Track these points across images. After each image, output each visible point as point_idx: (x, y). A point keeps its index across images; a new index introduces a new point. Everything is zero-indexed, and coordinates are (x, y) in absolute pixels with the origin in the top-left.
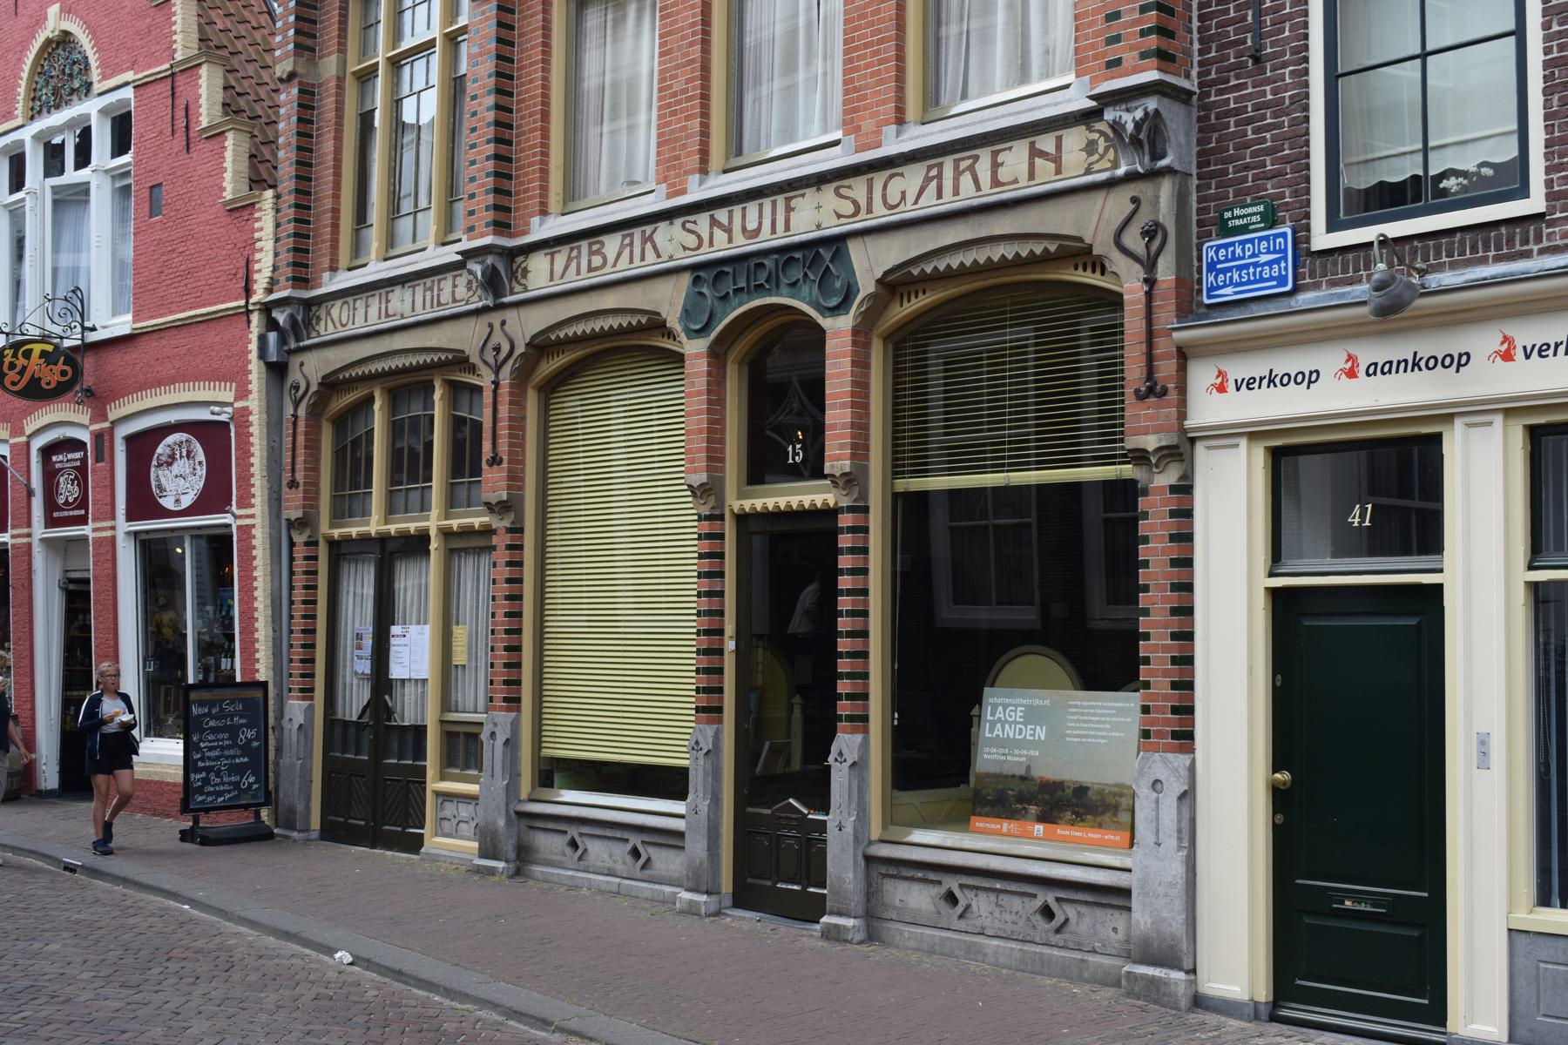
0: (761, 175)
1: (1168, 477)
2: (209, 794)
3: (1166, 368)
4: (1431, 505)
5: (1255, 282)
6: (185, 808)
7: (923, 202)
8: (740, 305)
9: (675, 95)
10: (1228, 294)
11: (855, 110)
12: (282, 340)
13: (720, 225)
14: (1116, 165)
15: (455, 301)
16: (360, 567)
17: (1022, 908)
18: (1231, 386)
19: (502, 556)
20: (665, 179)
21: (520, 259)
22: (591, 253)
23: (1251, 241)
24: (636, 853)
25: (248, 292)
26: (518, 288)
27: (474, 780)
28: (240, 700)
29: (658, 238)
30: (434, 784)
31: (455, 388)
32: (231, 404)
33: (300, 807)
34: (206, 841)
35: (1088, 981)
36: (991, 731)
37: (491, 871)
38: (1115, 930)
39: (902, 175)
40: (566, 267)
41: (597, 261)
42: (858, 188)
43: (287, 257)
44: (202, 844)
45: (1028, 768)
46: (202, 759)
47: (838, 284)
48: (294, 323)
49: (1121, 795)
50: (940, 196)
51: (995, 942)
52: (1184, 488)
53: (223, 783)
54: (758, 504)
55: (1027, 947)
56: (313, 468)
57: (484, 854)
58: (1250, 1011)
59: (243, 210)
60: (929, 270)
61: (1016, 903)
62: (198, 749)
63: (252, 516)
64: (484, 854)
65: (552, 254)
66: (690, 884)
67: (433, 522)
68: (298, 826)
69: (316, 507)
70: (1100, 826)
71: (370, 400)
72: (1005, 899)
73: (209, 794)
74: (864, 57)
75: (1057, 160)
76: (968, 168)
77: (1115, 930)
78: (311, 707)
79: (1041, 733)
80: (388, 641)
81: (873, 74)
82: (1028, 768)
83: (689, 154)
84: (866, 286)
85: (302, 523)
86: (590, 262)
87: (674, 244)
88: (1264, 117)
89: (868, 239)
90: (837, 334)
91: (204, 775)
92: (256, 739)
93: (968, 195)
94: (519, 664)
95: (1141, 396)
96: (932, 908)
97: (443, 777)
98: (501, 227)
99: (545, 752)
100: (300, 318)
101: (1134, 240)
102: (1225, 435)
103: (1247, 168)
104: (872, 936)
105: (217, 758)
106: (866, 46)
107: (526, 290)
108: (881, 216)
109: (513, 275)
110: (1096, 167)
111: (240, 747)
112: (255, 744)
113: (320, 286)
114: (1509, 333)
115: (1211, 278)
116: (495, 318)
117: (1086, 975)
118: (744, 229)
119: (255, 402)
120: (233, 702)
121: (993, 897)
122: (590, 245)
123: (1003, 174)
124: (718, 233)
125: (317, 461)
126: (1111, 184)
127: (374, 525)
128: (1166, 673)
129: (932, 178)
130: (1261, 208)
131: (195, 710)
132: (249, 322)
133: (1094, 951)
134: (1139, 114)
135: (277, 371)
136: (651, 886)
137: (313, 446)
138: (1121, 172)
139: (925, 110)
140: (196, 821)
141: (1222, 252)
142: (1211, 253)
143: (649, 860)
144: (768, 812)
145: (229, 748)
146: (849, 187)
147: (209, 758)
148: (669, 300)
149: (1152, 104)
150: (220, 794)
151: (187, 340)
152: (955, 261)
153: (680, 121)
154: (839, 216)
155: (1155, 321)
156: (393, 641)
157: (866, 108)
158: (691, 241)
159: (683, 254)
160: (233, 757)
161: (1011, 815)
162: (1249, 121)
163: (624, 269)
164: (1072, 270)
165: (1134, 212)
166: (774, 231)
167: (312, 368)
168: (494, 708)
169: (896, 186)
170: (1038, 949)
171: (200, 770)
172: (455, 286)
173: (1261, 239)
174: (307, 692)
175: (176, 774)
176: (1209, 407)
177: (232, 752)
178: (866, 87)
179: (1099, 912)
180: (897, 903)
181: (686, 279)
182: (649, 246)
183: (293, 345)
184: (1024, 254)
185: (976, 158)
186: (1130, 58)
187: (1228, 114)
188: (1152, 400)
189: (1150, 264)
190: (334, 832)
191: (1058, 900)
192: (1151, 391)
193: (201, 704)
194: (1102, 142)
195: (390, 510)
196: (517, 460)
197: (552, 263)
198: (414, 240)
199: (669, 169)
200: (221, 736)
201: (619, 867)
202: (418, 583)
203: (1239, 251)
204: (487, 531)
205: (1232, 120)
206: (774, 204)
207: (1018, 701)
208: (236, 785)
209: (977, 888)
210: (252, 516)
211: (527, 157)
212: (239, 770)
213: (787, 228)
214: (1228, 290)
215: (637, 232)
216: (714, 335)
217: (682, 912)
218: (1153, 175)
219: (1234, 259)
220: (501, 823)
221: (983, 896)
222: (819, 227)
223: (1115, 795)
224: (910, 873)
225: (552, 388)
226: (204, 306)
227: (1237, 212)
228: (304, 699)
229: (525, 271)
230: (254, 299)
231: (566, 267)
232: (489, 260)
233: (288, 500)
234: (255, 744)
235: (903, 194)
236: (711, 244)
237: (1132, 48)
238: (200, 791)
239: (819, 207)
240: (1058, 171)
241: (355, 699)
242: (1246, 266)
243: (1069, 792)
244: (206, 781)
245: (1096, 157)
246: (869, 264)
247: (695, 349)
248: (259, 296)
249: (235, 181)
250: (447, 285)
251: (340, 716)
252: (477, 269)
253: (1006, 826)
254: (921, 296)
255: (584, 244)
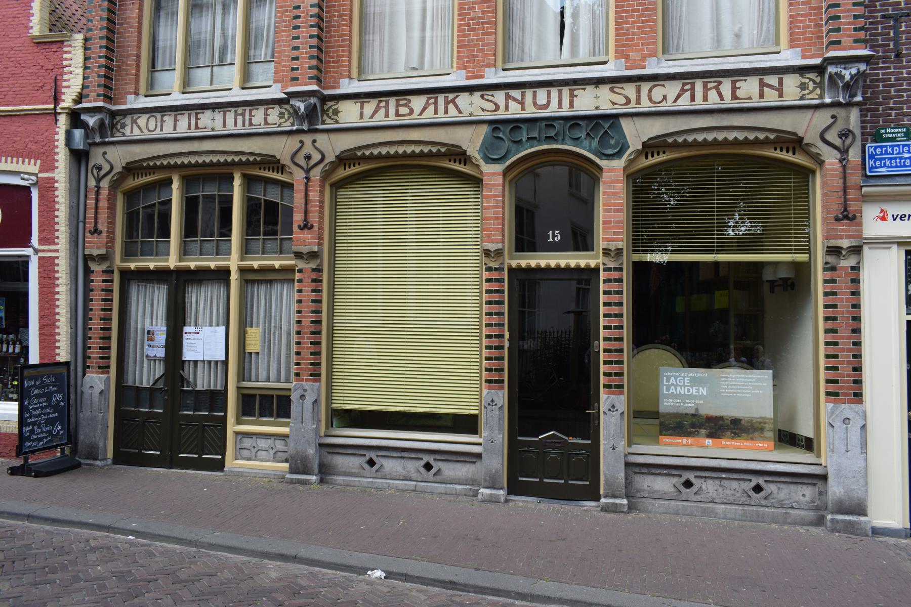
0: (549, 74)
1: (851, 262)
2: (34, 440)
3: (853, 207)
4: (20, 286)
5: (901, 166)
6: (19, 452)
7: (425, 115)
8: (531, 147)
9: (473, 19)
10: (883, 171)
11: (624, 46)
12: (87, 136)
13: (514, 99)
14: (821, 97)
15: (266, 123)
16: (203, 289)
17: (737, 488)
18: (890, 218)
19: (308, 286)
20: (465, 68)
21: (330, 104)
22: (398, 105)
23: (898, 146)
24: (428, 467)
25: (56, 100)
26: (328, 121)
27: (286, 425)
28: (54, 375)
29: (139, 121)
30: (232, 427)
31: (250, 181)
32: (36, 175)
33: (101, 445)
34: (40, 473)
35: (790, 524)
36: (668, 390)
37: (305, 483)
38: (804, 496)
39: (663, 86)
40: (375, 112)
41: (403, 110)
42: (630, 90)
43: (94, 80)
44: (36, 476)
45: (697, 410)
46: (30, 417)
47: (612, 142)
48: (97, 126)
49: (765, 423)
50: (436, 112)
51: (723, 506)
52: (856, 269)
53: (42, 432)
54: (524, 263)
55: (746, 508)
56: (112, 223)
57: (292, 471)
58: (904, 534)
59: (51, 44)
60: (151, 164)
61: (735, 484)
62: (28, 410)
63: (57, 251)
64: (292, 471)
65: (225, 113)
66: (487, 484)
67: (233, 262)
68: (100, 457)
69: (113, 248)
70: (752, 439)
71: (169, 182)
72: (726, 483)
73: (34, 440)
74: (632, 17)
75: (522, 103)
76: (714, 88)
77: (804, 496)
78: (108, 378)
79: (704, 391)
80: (182, 336)
81: (638, 28)
82: (697, 410)
83: (486, 55)
84: (635, 145)
85: (102, 258)
86: (397, 111)
87: (471, 106)
88: (902, 85)
89: (635, 119)
90: (611, 170)
91: (31, 428)
92: (62, 401)
93: (714, 100)
94: (317, 349)
95: (92, 234)
96: (673, 489)
97: (239, 422)
98: (108, 98)
99: (335, 406)
100: (107, 122)
101: (832, 137)
102: (883, 242)
103: (892, 109)
104: (631, 508)
105: (39, 415)
106: (633, 11)
107: (337, 122)
108: (646, 105)
109: (113, 126)
110: (808, 97)
111: (53, 407)
112: (62, 404)
113: (125, 103)
114: (884, 208)
115: (872, 162)
116: (307, 139)
117: (789, 520)
118: (535, 104)
119: (61, 174)
120: (49, 376)
121: (717, 482)
122: (397, 101)
123: (739, 93)
124: (512, 104)
125: (114, 218)
126: (823, 106)
127: (172, 262)
128: (849, 363)
129: (687, 90)
130: (904, 130)
131: (27, 383)
132: (57, 120)
133: (792, 508)
134: (854, 71)
135: (79, 157)
136: (444, 485)
137: (112, 208)
138: (295, 128)
139: (184, 87)
140: (26, 460)
141: (878, 150)
142: (871, 150)
143: (439, 470)
144: (537, 439)
145: (46, 407)
146: (622, 88)
147: (35, 416)
148: (471, 141)
149: (863, 67)
150: (40, 440)
151: (15, 126)
152: (700, 137)
153: (478, 35)
154: (483, 110)
155: (847, 181)
156: (185, 336)
157: (633, 45)
158: (491, 106)
159: (482, 113)
160: (48, 414)
161: (688, 434)
162: (892, 86)
163: (429, 116)
164: (773, 150)
165: (833, 123)
166: (244, 125)
167: (118, 157)
168: (302, 380)
169: (658, 93)
170: (755, 508)
171: (28, 425)
172: (266, 115)
173: (904, 146)
174: (105, 368)
175: (14, 428)
176: (872, 224)
177: (48, 411)
178: (633, 34)
179: (793, 487)
180: (646, 487)
181: (484, 129)
182: (451, 106)
183: (98, 140)
184: (193, 162)
185: (720, 83)
186: (93, 95)
187: (878, 80)
188: (306, 230)
189: (844, 151)
190: (123, 457)
191: (766, 481)
192: (306, 226)
193: (30, 379)
194: (286, 113)
195: (184, 252)
196: (111, 233)
197: (362, 108)
198: (211, 84)
199: (468, 62)
200: (41, 400)
201: (414, 475)
202: (200, 299)
203: (889, 150)
204: (291, 270)
205: (881, 84)
206: (560, 92)
207: (685, 374)
208: (50, 432)
209: (706, 477)
210: (57, 251)
211: (335, 41)
212: (51, 422)
213: (571, 105)
214: (884, 169)
215: (441, 98)
216: (508, 163)
217: (484, 501)
218: (849, 105)
219: (886, 153)
220: (311, 451)
221: (710, 482)
222: (597, 108)
223: (760, 423)
224: (658, 471)
225: (338, 186)
226: (8, 105)
227: (889, 130)
228: (103, 373)
229: (336, 112)
230: (62, 105)
231: (375, 112)
232: (313, 100)
233: (90, 242)
234: (62, 404)
235: (665, 97)
236: (507, 108)
237: (849, 36)
238: (28, 439)
239: (597, 97)
240: (781, 96)
241: (147, 372)
242: (895, 158)
243: (728, 422)
244: (32, 432)
245: (807, 91)
246: (636, 134)
247: (492, 172)
248: (67, 101)
249: (41, 22)
250: (230, 116)
251: (130, 383)
252: (302, 106)
253: (684, 440)
254: (357, 166)
255: (392, 101)
